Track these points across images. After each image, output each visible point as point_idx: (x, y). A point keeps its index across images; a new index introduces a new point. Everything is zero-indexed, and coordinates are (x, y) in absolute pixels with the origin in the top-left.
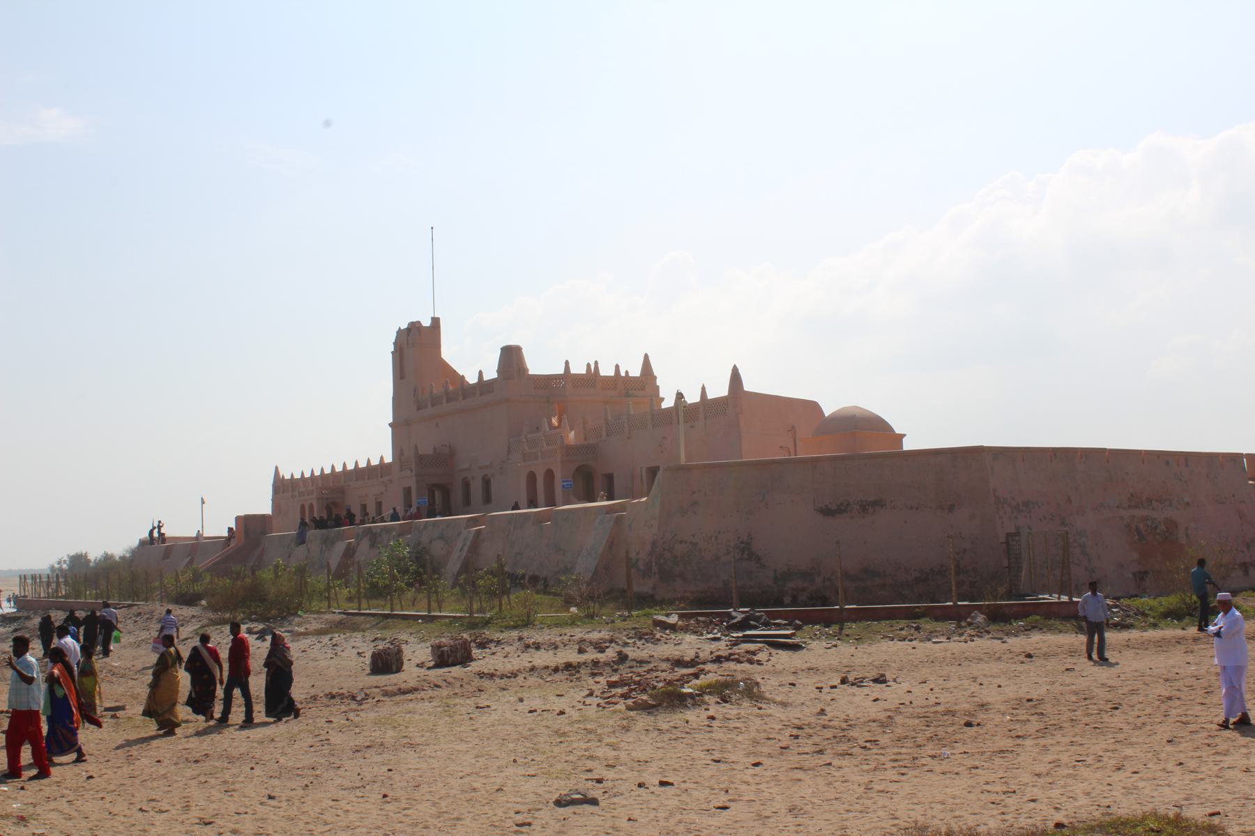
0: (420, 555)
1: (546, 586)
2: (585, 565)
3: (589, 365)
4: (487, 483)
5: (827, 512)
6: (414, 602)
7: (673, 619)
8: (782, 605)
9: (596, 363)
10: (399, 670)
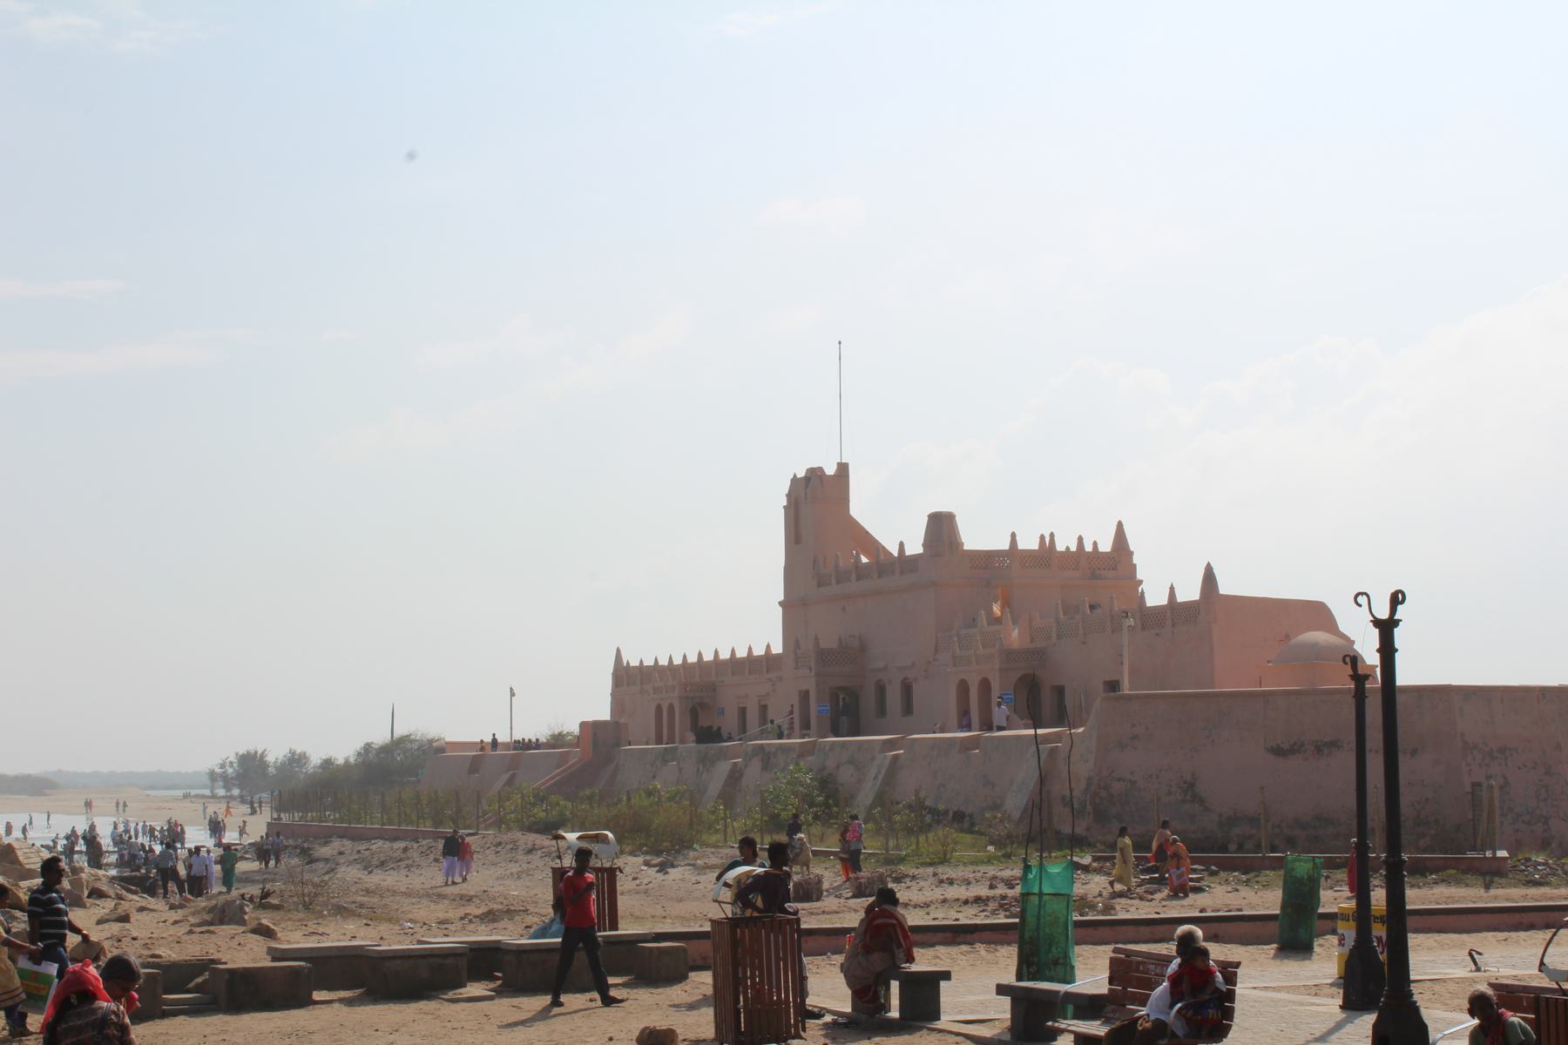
0: (827, 783)
1: (973, 824)
2: (1015, 803)
3: (1042, 538)
4: (907, 689)
5: (1278, 752)
6: (822, 839)
7: (1086, 860)
8: (1226, 851)
9: (1052, 535)
10: (818, 899)
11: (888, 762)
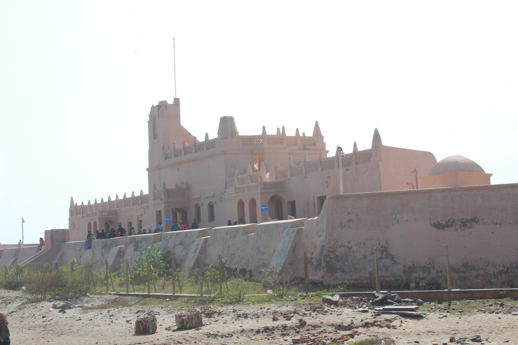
0: (167, 256)
1: (251, 276)
2: (277, 262)
3: (278, 129)
4: (211, 208)
5: (439, 226)
6: (163, 287)
7: (336, 298)
9: (283, 128)
10: (154, 332)
11: (202, 242)
